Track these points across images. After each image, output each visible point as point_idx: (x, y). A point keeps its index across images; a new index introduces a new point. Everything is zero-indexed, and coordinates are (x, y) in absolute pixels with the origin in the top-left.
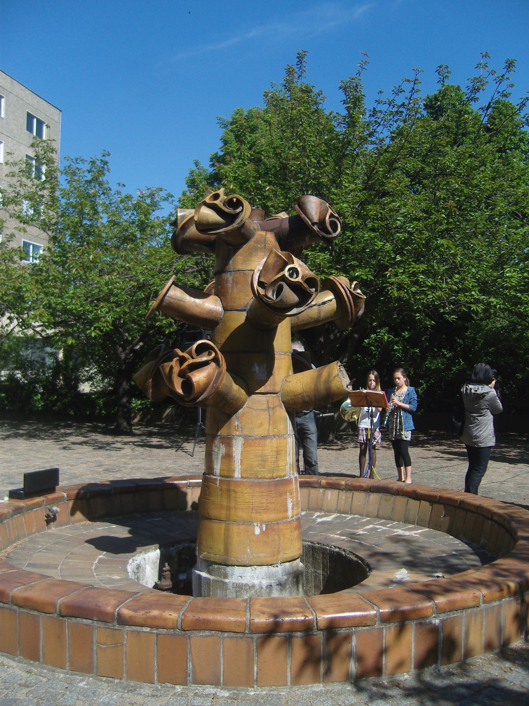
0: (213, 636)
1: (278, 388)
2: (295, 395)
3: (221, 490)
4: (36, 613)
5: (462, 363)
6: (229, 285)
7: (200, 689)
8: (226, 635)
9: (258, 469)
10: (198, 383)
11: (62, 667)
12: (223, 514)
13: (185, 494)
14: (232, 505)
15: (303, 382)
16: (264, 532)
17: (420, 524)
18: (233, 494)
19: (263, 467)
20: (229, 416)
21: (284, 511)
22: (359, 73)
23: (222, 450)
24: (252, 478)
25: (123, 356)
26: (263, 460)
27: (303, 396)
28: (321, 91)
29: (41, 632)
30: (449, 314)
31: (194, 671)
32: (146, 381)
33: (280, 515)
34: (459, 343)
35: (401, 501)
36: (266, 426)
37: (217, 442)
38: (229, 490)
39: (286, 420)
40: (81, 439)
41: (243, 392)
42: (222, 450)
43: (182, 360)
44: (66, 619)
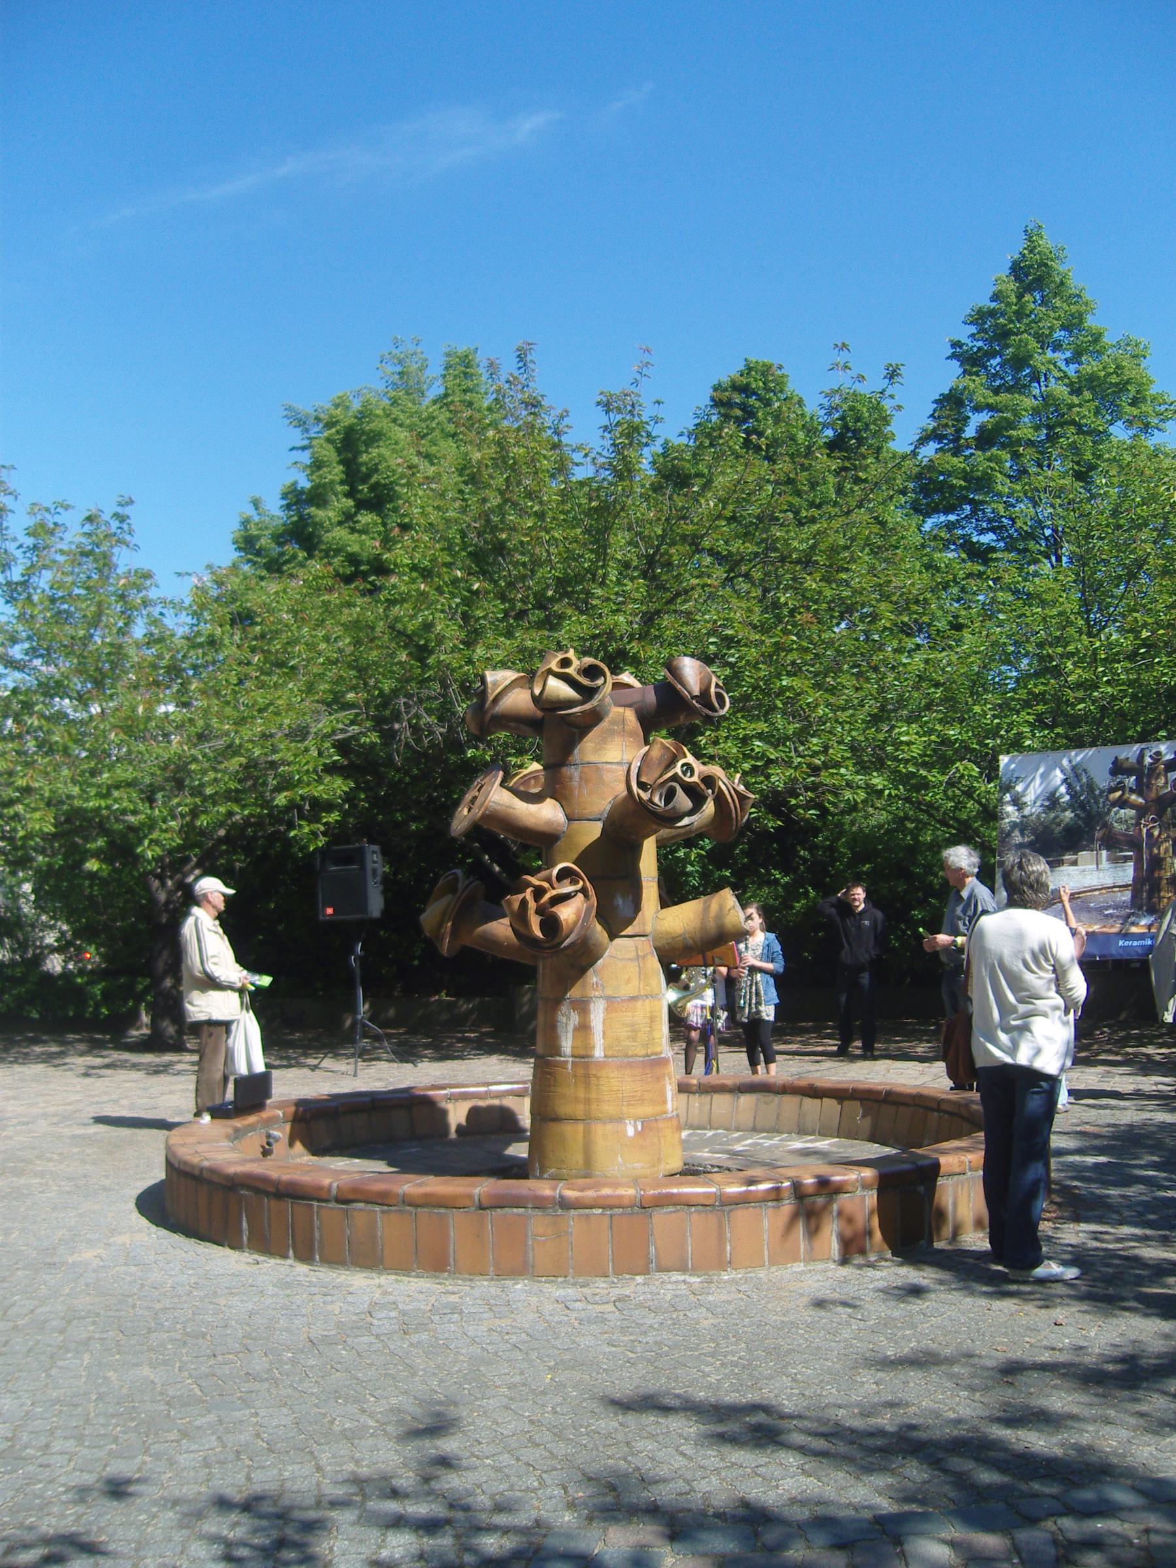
1: (649, 929)
3: (575, 1076)
4: (443, 1210)
5: (812, 893)
6: (575, 784)
7: (664, 1276)
8: (693, 1209)
9: (627, 1043)
12: (579, 1110)
13: (444, 1113)
14: (593, 1095)
15: (682, 919)
17: (824, 1133)
18: (593, 1080)
19: (634, 1039)
22: (636, 383)
23: (575, 1019)
25: (162, 897)
26: (634, 1030)
28: (566, 411)
30: (807, 808)
31: (657, 1257)
32: (441, 924)
33: (659, 1108)
34: (802, 858)
35: (790, 1101)
36: (635, 982)
37: (564, 1008)
38: (587, 1076)
39: (659, 975)
40: (98, 1061)
42: (575, 1019)
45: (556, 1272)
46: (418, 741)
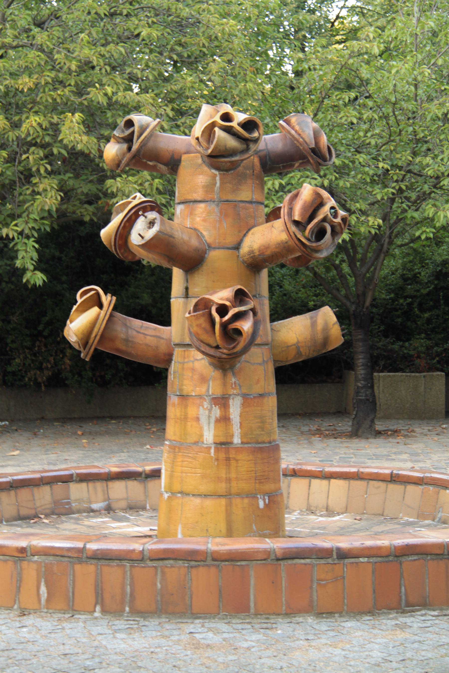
0: (419, 559)
4: (243, 563)
24: (253, 443)
29: (252, 582)
44: (282, 562)
46: (81, 62)
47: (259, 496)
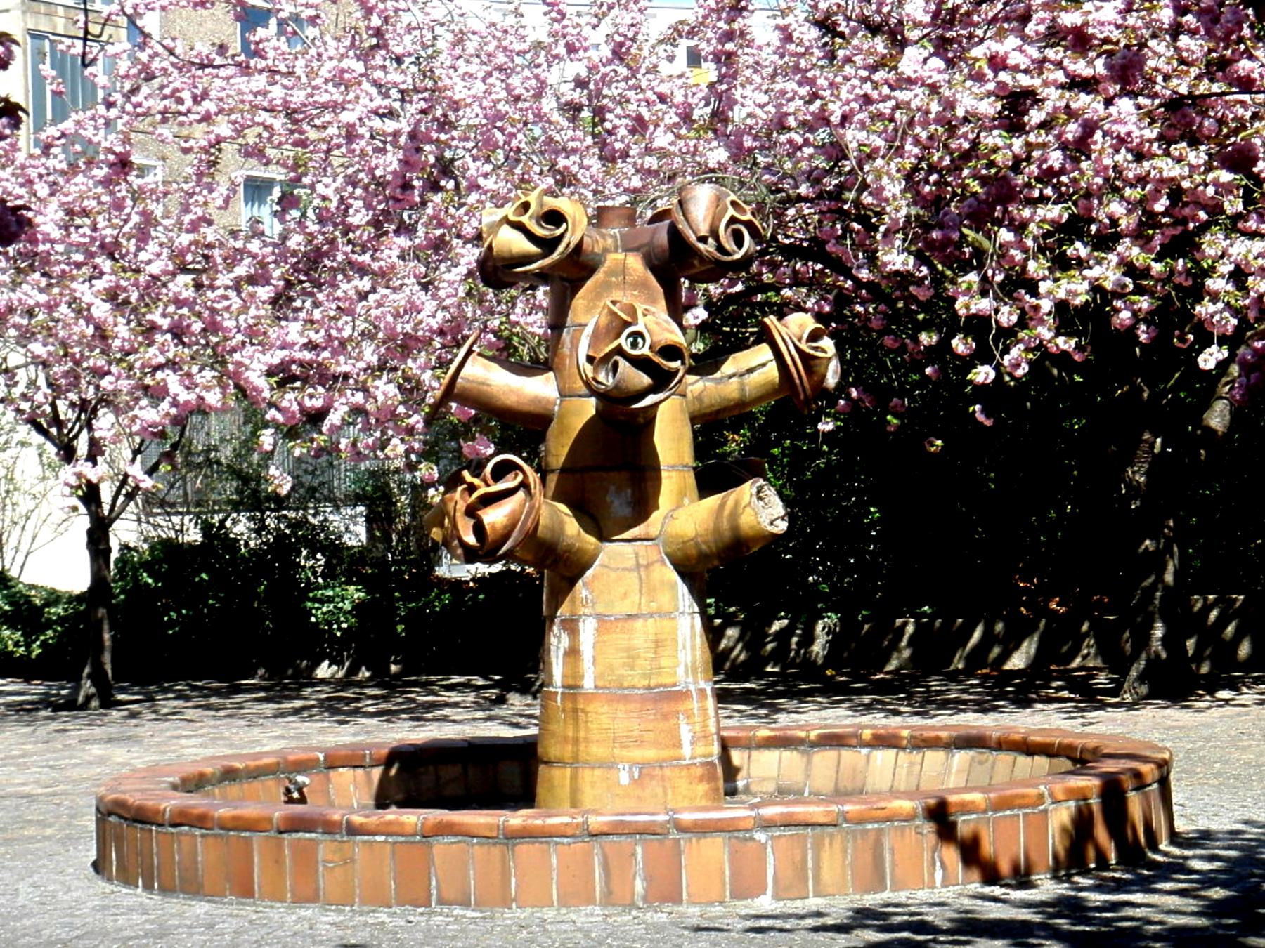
2: (684, 542)
3: (564, 710)
4: (248, 834)
8: (475, 840)
9: (622, 672)
10: (493, 526)
11: (282, 901)
16: (635, 781)
20: (572, 582)
21: (674, 746)
26: (632, 657)
27: (697, 544)
29: (256, 859)
33: (665, 753)
38: (575, 710)
39: (673, 586)
41: (592, 540)
42: (565, 641)
43: (472, 488)
44: (285, 836)
45: (345, 900)
47: (620, 766)
